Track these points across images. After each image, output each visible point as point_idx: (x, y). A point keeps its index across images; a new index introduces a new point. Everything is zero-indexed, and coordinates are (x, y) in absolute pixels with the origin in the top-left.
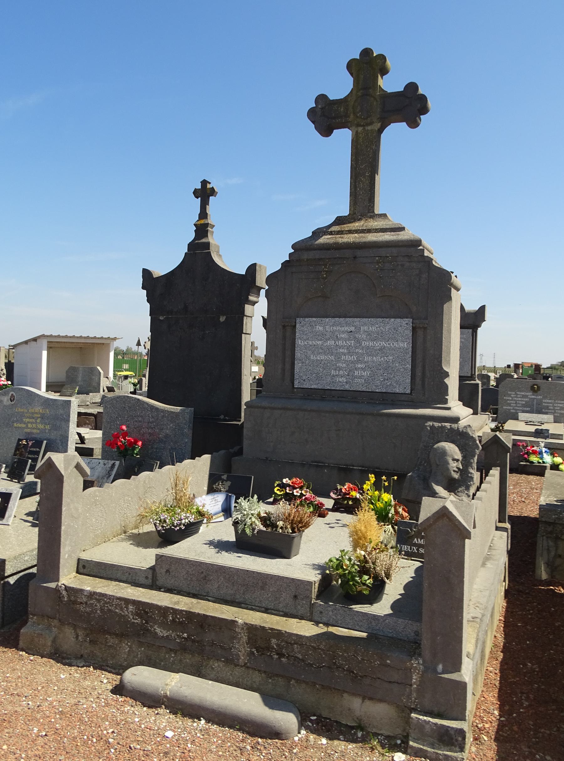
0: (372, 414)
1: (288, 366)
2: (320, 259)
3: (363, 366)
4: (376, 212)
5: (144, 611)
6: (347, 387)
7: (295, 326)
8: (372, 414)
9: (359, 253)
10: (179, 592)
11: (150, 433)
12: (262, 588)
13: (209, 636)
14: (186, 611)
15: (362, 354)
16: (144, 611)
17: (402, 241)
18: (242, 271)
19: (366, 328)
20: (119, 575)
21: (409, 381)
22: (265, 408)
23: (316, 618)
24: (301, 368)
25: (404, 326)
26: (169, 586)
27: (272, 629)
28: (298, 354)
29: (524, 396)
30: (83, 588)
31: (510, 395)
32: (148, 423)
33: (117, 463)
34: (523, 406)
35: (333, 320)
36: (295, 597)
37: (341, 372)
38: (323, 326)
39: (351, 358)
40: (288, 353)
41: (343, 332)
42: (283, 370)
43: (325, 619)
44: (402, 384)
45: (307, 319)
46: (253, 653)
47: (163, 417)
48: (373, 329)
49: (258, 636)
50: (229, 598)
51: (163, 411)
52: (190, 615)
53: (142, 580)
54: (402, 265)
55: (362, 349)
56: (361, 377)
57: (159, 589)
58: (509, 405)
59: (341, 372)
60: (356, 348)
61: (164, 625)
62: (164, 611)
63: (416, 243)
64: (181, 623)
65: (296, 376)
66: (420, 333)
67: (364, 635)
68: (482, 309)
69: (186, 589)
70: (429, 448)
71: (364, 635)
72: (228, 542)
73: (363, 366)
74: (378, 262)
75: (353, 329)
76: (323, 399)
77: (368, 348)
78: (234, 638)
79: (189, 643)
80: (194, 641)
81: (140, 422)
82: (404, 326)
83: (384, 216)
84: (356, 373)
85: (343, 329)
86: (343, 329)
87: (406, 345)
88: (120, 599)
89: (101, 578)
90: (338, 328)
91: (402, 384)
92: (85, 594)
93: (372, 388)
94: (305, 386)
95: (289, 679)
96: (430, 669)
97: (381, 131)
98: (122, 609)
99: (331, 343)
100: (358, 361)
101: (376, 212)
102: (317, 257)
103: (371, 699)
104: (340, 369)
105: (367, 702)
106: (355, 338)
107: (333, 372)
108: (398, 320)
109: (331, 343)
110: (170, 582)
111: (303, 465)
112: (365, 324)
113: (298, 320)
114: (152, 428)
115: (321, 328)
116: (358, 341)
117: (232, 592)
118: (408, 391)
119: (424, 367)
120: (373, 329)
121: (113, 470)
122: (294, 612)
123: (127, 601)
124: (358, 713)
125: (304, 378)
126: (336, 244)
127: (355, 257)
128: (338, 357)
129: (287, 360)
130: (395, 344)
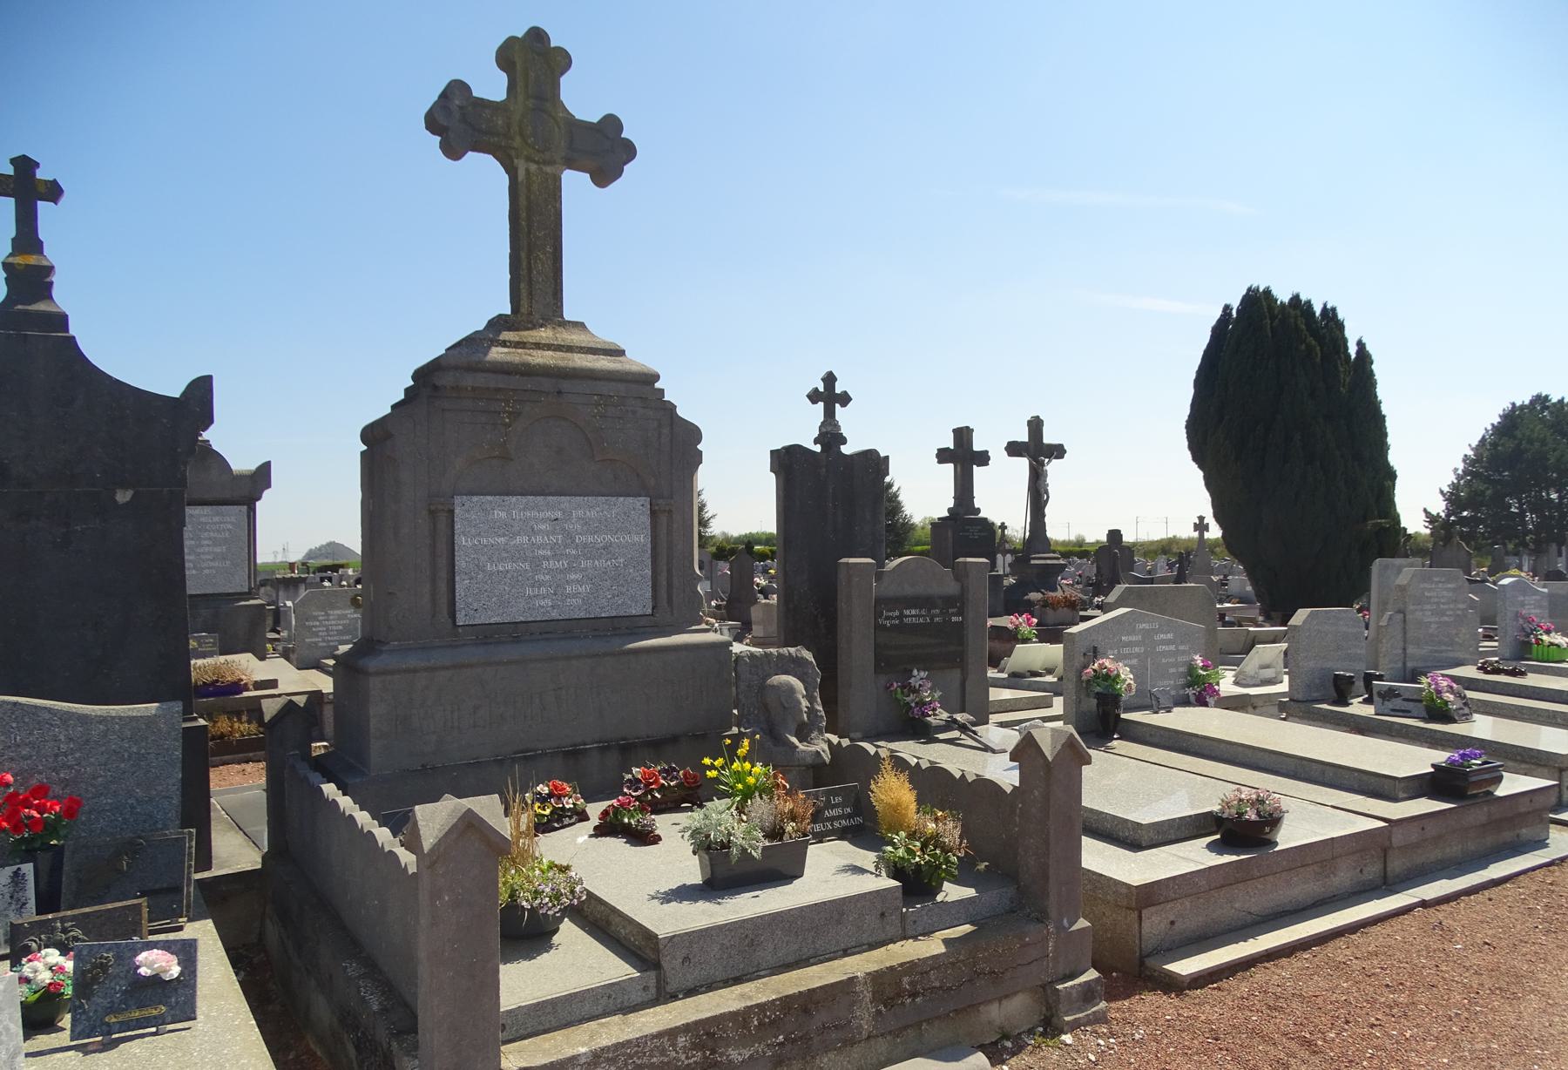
0: (613, 654)
1: (443, 587)
2: (498, 390)
3: (578, 576)
4: (567, 316)
5: (708, 1034)
6: (555, 615)
7: (452, 512)
8: (613, 654)
9: (566, 385)
10: (710, 987)
11: (62, 781)
12: (839, 922)
13: (821, 1017)
14: (780, 999)
15: (577, 557)
16: (708, 1034)
17: (628, 373)
18: (175, 390)
19: (580, 513)
20: (587, 1008)
21: (649, 594)
22: (415, 671)
23: (910, 933)
24: (468, 588)
25: (638, 507)
26: (690, 985)
27: (901, 965)
28: (461, 563)
29: (340, 617)
30: (575, 1052)
31: (316, 618)
32: (56, 756)
33: (28, 869)
34: (340, 633)
35: (524, 499)
36: (883, 914)
37: (543, 590)
38: (505, 510)
39: (559, 565)
40: (442, 562)
41: (543, 520)
42: (434, 593)
43: (920, 929)
44: (638, 602)
45: (475, 499)
46: (879, 1012)
47: (105, 734)
48: (592, 514)
49: (886, 985)
50: (791, 959)
51: (103, 720)
52: (787, 1003)
53: (637, 997)
54: (634, 412)
55: (577, 547)
56: (575, 596)
57: (674, 997)
58: (316, 634)
59: (543, 590)
60: (566, 546)
61: (744, 1042)
62: (740, 1018)
63: (648, 379)
64: (772, 1022)
65: (459, 605)
66: (663, 519)
67: (967, 928)
68: (265, 469)
69: (720, 975)
70: (763, 688)
71: (967, 928)
72: (694, 887)
73: (578, 576)
74: (597, 405)
75: (559, 514)
76: (517, 640)
77: (585, 545)
78: (853, 1003)
79: (789, 1047)
80: (794, 1041)
81: (24, 758)
82: (638, 507)
83: (580, 326)
84: (569, 589)
85: (542, 515)
86: (542, 515)
87: (643, 539)
88: (660, 1035)
89: (546, 1032)
90: (534, 513)
91: (638, 602)
92: (583, 1061)
93: (596, 612)
94: (477, 622)
95: (919, 1024)
96: (1060, 928)
97: (511, 170)
98: (663, 1052)
99: (522, 540)
100: (570, 569)
101: (567, 316)
102: (492, 385)
103: (1006, 996)
104: (541, 584)
105: (1004, 1002)
106: (564, 529)
107: (529, 591)
108: (630, 499)
109: (522, 540)
110: (692, 977)
111: (500, 762)
112: (579, 506)
113: (458, 500)
114: (70, 767)
115: (503, 515)
116: (569, 536)
117: (796, 947)
118: (649, 611)
119: (669, 571)
120: (592, 514)
121: (23, 889)
122: (883, 937)
123: (672, 1033)
124: (998, 1022)
125: (475, 606)
126: (527, 365)
127: (559, 392)
128: (536, 563)
129: (664, 574)
130: (627, 537)
